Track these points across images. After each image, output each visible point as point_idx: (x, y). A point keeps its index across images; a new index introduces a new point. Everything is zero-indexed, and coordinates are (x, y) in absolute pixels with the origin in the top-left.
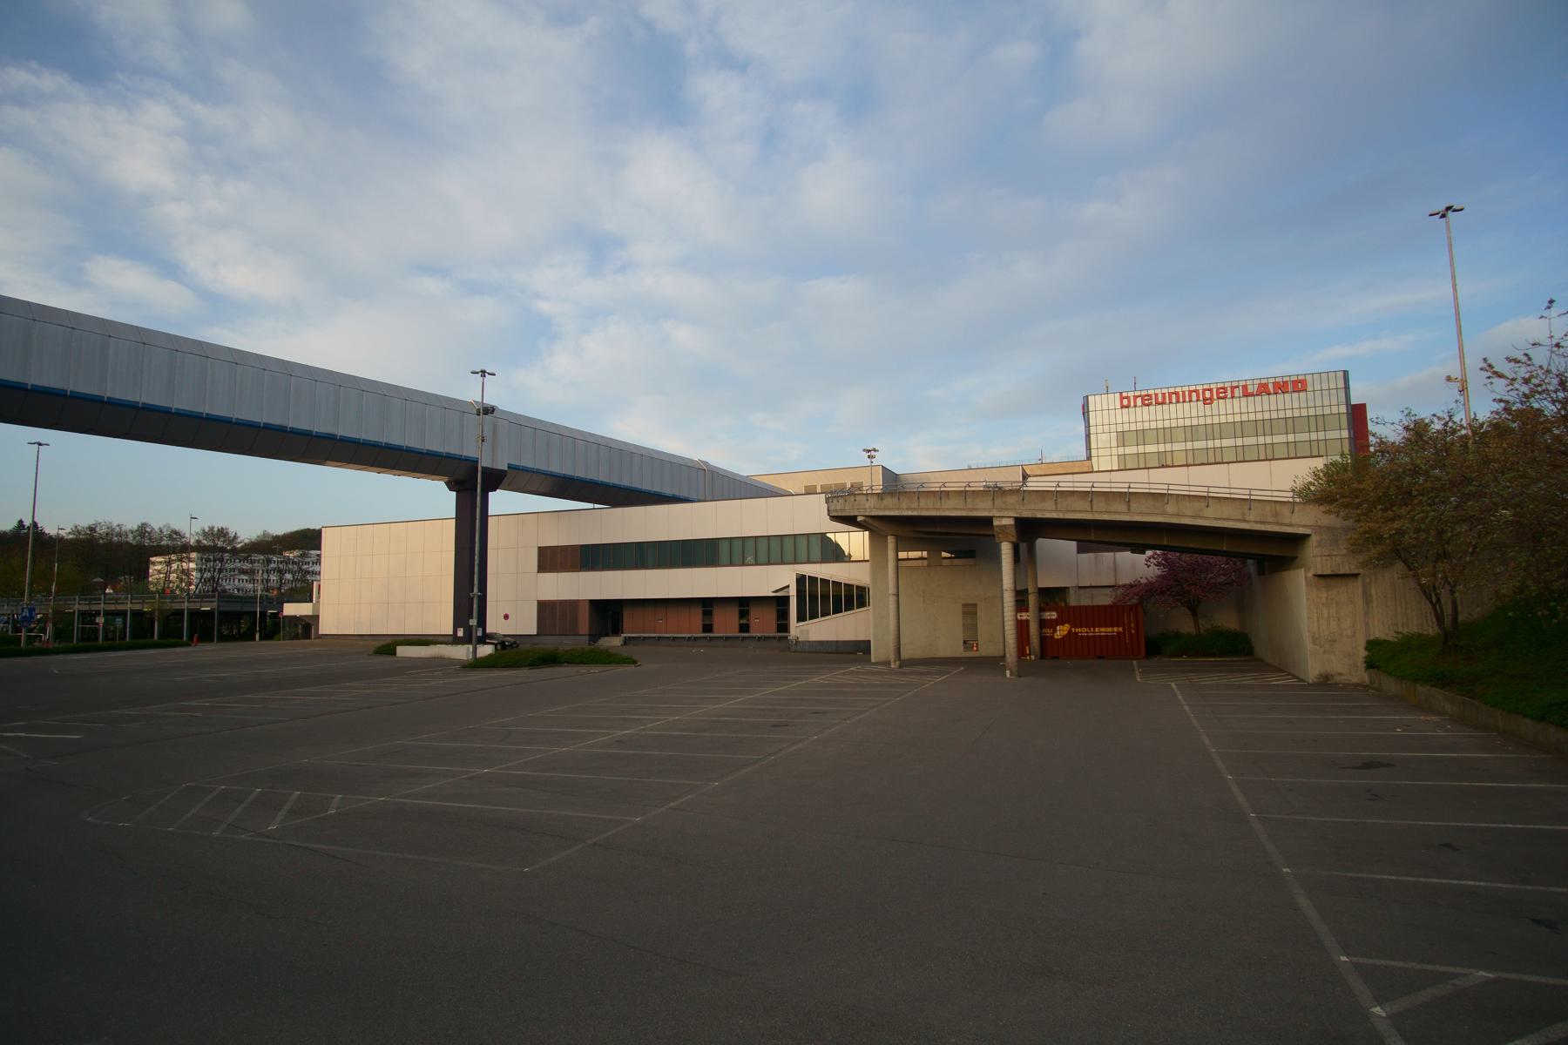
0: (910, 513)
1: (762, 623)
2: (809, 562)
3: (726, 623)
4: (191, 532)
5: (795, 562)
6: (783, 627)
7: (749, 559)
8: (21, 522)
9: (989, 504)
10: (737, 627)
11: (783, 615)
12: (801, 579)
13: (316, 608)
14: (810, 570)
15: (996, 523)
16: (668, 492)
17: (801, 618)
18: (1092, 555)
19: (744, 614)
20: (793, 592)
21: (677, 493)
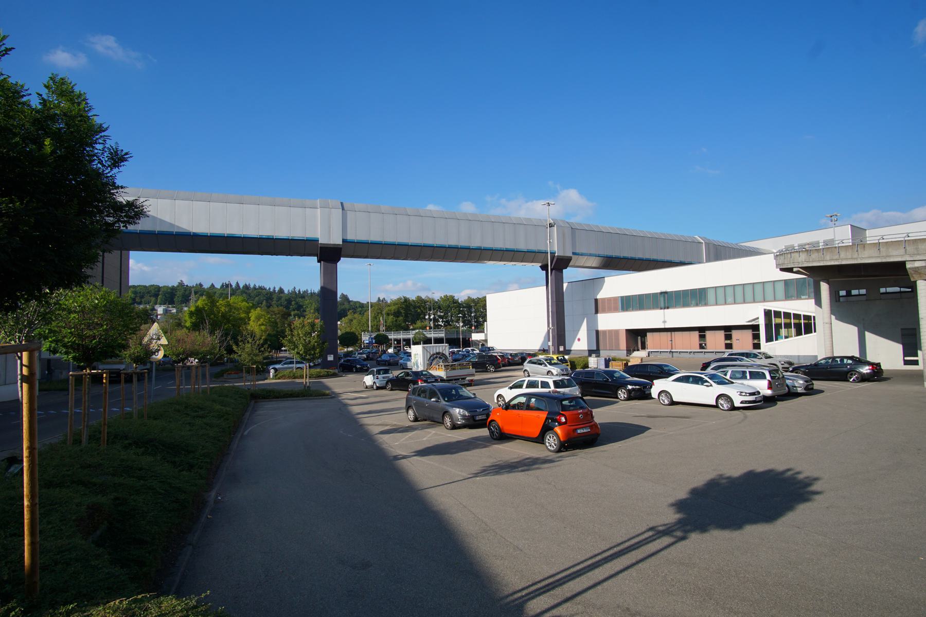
0: (833, 263)
1: (742, 342)
2: (775, 300)
3: (716, 341)
4: (437, 296)
5: (764, 301)
6: (757, 346)
7: (730, 299)
8: (213, 285)
9: (902, 251)
10: (724, 346)
11: (756, 336)
12: (767, 313)
13: (486, 335)
14: (774, 306)
15: (908, 266)
16: (676, 260)
17: (769, 339)
18: (168, 202)
19: (702, 337)
20: (762, 323)
21: (682, 260)
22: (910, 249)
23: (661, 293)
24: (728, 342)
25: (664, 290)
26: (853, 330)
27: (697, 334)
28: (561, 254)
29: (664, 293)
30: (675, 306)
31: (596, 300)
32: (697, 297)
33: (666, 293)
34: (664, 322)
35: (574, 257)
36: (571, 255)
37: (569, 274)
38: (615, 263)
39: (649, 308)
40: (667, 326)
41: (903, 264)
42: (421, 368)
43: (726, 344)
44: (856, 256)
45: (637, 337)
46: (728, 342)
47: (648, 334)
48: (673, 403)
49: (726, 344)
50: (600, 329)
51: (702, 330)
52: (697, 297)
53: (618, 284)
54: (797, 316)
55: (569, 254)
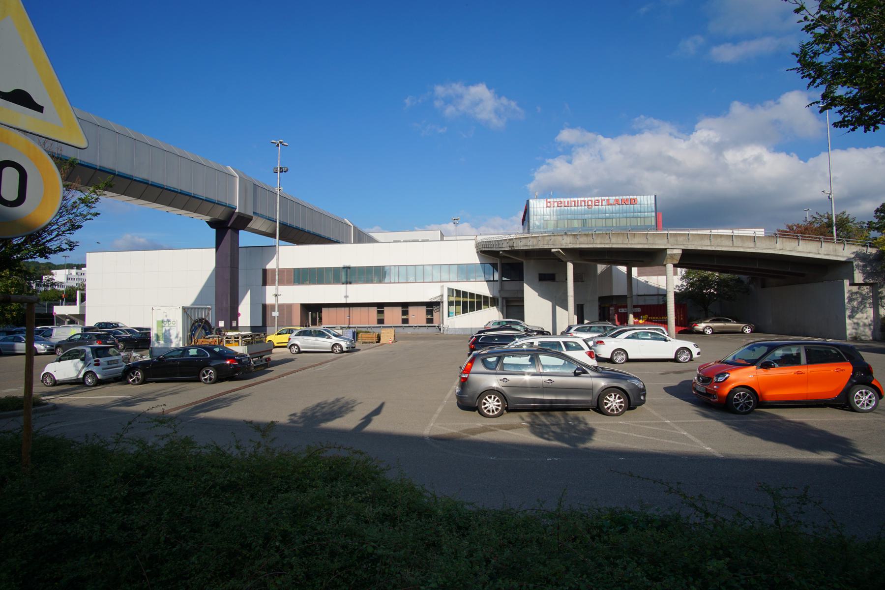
0: (603, 246)
12: (451, 291)
13: (83, 308)
15: (669, 252)
22: (671, 240)
23: (344, 268)
24: (405, 317)
25: (347, 265)
26: (548, 304)
27: (375, 309)
28: (242, 212)
29: (347, 268)
30: (356, 282)
31: (265, 271)
32: (376, 274)
33: (349, 268)
34: (346, 297)
35: (254, 217)
36: (251, 214)
37: (246, 238)
38: (295, 235)
39: (329, 283)
40: (349, 301)
41: (665, 250)
42: (177, 342)
43: (403, 320)
44: (626, 241)
45: (312, 312)
46: (405, 317)
47: (324, 310)
48: (628, 360)
49: (403, 320)
50: (267, 302)
51: (381, 306)
52: (376, 274)
53: (290, 256)
54: (472, 295)
55: (250, 213)
